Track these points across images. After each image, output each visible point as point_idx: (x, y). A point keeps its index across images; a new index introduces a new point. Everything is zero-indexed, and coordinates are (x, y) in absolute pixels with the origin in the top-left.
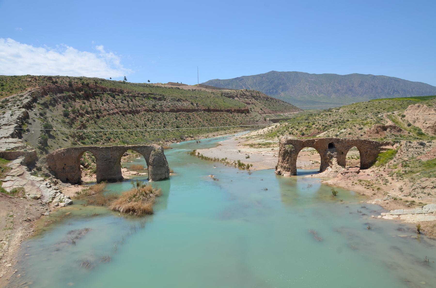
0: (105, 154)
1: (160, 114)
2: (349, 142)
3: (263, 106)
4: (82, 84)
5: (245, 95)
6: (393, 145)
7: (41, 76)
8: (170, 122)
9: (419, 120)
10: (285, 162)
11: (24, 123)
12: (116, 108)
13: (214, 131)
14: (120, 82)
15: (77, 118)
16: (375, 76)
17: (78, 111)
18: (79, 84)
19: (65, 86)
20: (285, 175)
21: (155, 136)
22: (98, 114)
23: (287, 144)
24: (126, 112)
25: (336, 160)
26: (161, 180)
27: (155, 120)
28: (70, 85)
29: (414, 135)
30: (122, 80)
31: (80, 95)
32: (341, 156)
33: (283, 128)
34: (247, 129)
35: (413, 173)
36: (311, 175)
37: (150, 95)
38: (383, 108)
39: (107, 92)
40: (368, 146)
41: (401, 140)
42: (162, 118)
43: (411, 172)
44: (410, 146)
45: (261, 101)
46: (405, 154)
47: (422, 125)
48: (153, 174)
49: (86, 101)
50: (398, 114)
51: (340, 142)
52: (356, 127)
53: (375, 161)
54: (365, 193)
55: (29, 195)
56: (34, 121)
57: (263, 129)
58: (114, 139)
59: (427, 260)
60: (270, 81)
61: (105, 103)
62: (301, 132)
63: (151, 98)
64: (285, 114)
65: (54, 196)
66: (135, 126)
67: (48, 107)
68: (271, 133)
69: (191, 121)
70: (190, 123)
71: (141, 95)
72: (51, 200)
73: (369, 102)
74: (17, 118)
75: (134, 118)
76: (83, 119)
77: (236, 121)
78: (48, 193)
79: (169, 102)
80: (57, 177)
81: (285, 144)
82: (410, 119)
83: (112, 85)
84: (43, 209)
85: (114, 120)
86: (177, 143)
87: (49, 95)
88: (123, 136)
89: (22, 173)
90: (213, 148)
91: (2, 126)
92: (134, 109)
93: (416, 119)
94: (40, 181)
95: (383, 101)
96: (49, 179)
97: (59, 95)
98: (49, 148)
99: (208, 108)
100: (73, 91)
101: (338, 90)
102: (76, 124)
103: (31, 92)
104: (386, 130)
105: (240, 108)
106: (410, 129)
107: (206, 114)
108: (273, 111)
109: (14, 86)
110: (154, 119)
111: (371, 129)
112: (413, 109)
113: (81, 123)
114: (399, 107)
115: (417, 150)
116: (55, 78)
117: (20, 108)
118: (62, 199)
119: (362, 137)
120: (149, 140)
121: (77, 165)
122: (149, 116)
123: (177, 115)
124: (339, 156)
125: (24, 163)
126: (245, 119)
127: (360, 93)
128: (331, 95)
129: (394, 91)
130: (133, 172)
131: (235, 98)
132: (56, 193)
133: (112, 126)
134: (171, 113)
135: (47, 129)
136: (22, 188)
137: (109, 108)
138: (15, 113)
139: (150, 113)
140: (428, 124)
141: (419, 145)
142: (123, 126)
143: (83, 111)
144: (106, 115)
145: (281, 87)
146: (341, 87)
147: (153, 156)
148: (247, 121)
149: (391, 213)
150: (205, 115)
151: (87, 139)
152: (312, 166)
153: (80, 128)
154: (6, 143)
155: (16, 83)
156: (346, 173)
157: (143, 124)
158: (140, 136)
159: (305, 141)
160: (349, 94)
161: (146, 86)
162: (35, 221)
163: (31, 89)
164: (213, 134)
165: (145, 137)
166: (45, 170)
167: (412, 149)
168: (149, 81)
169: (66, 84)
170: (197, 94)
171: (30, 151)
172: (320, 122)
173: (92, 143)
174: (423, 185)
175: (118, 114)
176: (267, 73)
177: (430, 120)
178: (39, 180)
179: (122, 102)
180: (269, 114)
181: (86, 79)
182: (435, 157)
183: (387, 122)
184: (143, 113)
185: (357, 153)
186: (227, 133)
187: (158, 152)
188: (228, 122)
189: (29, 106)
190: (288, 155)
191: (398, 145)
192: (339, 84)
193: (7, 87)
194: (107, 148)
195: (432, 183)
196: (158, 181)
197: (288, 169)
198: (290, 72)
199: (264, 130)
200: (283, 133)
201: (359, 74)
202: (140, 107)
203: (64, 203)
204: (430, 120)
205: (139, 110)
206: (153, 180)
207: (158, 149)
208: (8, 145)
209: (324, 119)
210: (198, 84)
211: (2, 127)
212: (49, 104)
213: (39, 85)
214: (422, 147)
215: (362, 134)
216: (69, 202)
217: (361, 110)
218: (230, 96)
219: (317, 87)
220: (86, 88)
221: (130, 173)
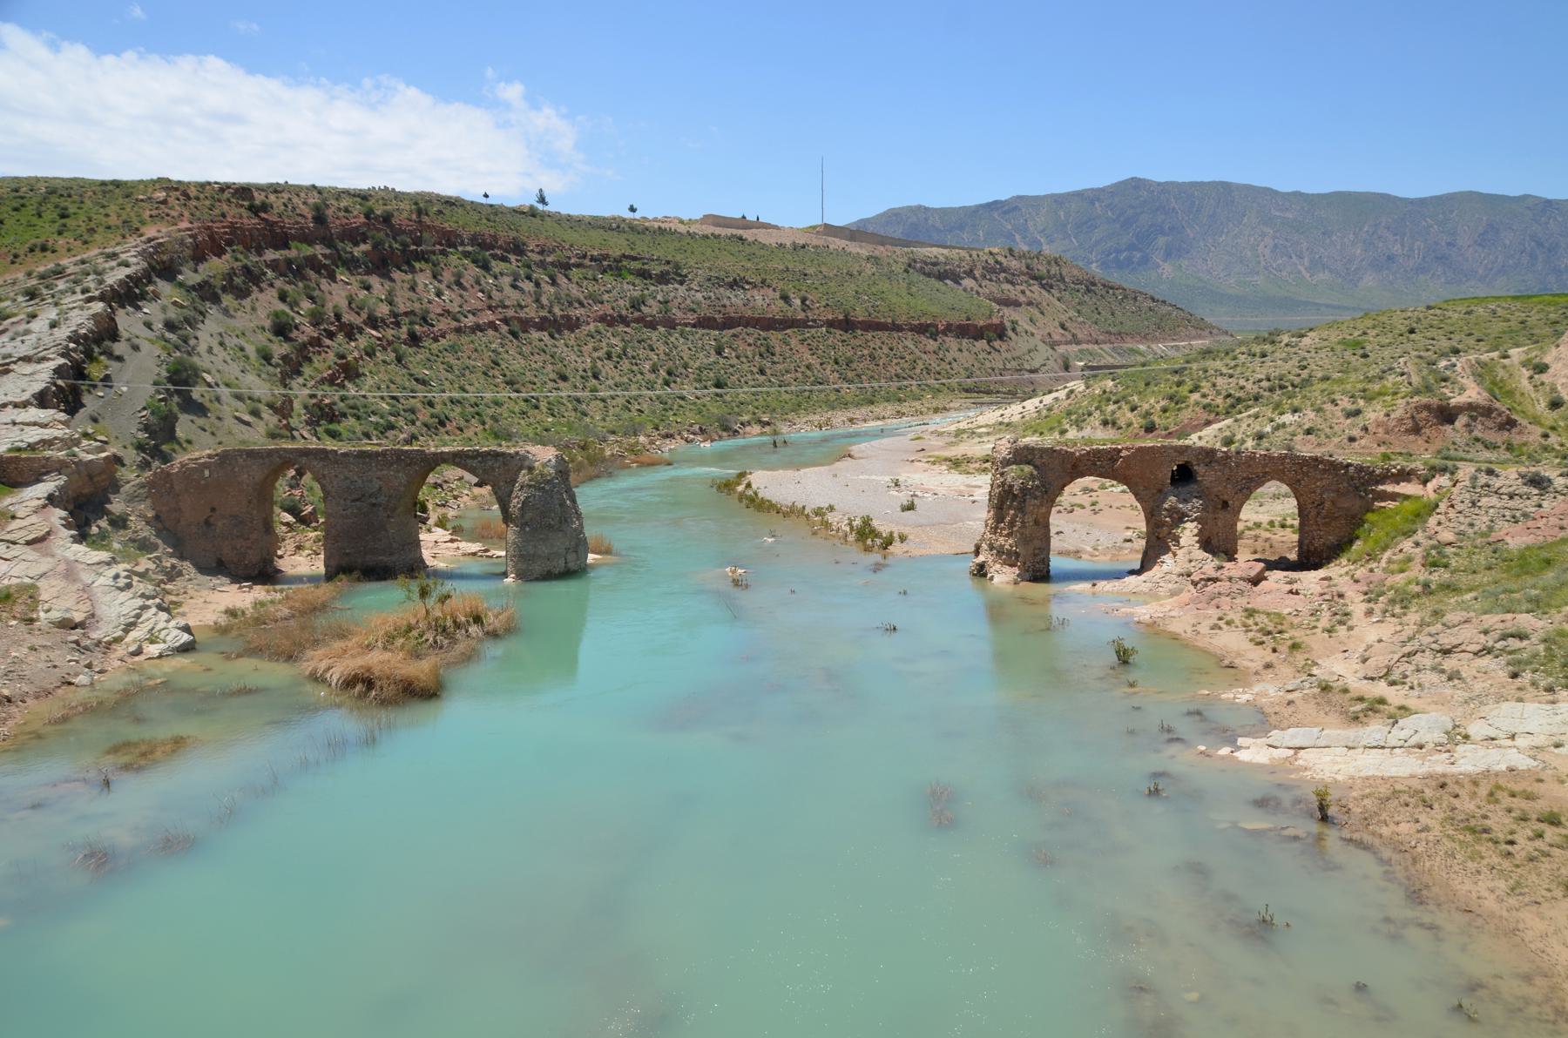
0: (356, 478)
1: (657, 333)
2: (1252, 463)
3: (1072, 313)
4: (367, 216)
5: (1004, 271)
6: (1425, 482)
7: (209, 183)
8: (692, 363)
10: (1001, 529)
11: (95, 354)
12: (490, 308)
13: (858, 405)
14: (516, 211)
15: (328, 342)
16: (1549, 202)
17: (338, 316)
18: (355, 217)
19: (297, 223)
21: (626, 415)
22: (417, 327)
23: (1013, 463)
24: (526, 324)
25: (1196, 531)
26: (548, 576)
27: (634, 358)
28: (320, 219)
29: (1562, 445)
30: (531, 200)
31: (353, 256)
32: (1221, 514)
33: (1093, 398)
34: (986, 399)
35: (1454, 590)
36: (1092, 582)
37: (624, 263)
38: (1477, 335)
39: (460, 249)
41: (1459, 464)
42: (662, 348)
43: (1448, 587)
44: (1489, 486)
45: (1066, 295)
46: (1462, 519)
48: (521, 556)
49: (374, 280)
50: (1524, 357)
51: (1216, 461)
52: (1337, 405)
53: (1351, 542)
54: (1237, 662)
55: (48, 611)
56: (136, 348)
57: (1025, 404)
58: (462, 423)
59: (1268, 918)
60: (1122, 219)
61: (449, 287)
62: (1144, 417)
63: (630, 272)
64: (1154, 346)
65: (132, 620)
66: (553, 376)
67: (216, 299)
68: (1046, 417)
69: (774, 363)
70: (768, 372)
71: (591, 260)
72: (120, 633)
73: (1429, 308)
74: (69, 337)
75: (556, 346)
76: (353, 344)
78: (115, 607)
80: (182, 553)
83: (485, 221)
84: (77, 662)
85: (476, 350)
86: (702, 445)
87: (227, 256)
88: (499, 410)
89: (43, 533)
90: (816, 469)
91: (15, 363)
92: (557, 311)
94: (98, 564)
95: (1486, 308)
96: (149, 559)
97: (270, 255)
98: (176, 447)
99: (845, 316)
100: (328, 241)
101: (1390, 258)
102: (316, 364)
103: (152, 243)
104: (1451, 422)
105: (968, 319)
106: (1555, 421)
107: (834, 338)
108: (1110, 333)
109: (105, 219)
110: (630, 352)
111: (1392, 416)
113: (339, 362)
114: (1544, 332)
115: (1511, 504)
116: (263, 190)
117: (90, 300)
118: (160, 631)
119: (1353, 444)
120: (599, 428)
121: (255, 512)
122: (614, 341)
123: (723, 340)
124: (1211, 516)
125: (60, 496)
126: (987, 362)
127: (1480, 271)
130: (469, 544)
131: (962, 282)
132: (144, 608)
133: (464, 375)
134: (701, 331)
135: (181, 378)
136: (33, 586)
137: (461, 306)
138: (66, 319)
139: (621, 328)
141: (1525, 484)
142: (508, 373)
143: (359, 314)
144: (445, 333)
146: (1402, 245)
148: (993, 370)
149: (1270, 741)
150: (830, 342)
151: (352, 421)
152: (1121, 548)
153: (331, 381)
154: (14, 423)
155: (112, 209)
156: (1209, 580)
157: (585, 371)
158: (565, 414)
159: (1084, 455)
161: (618, 227)
162: (30, 701)
163: (159, 231)
164: (852, 416)
165: (588, 420)
166: (141, 525)
167: (1494, 500)
168: (632, 209)
169: (305, 214)
170: (809, 263)
171: (91, 457)
172: (1220, 381)
173: (367, 436)
174: (1447, 640)
175: (496, 329)
178: (96, 560)
179: (514, 287)
180: (1090, 346)
181: (383, 199)
182: (1562, 534)
183: (1463, 389)
185: (1290, 506)
186: (904, 414)
187: (542, 475)
188: (918, 371)
189: (129, 295)
190: (1011, 503)
191: (1443, 480)
192: (1396, 235)
193: (77, 223)
194: (362, 455)
195: (1482, 636)
196: (537, 579)
197: (1009, 558)
199: (1024, 408)
200: (1085, 420)
203: (162, 646)
205: (578, 319)
206: (522, 576)
207: (544, 465)
208: (18, 432)
209: (1239, 370)
210: (820, 223)
211: (13, 366)
212: (224, 289)
213: (192, 215)
214: (1536, 491)
215: (1356, 432)
216: (182, 641)
217: (1387, 341)
218: (945, 271)
220: (379, 230)
221: (458, 548)
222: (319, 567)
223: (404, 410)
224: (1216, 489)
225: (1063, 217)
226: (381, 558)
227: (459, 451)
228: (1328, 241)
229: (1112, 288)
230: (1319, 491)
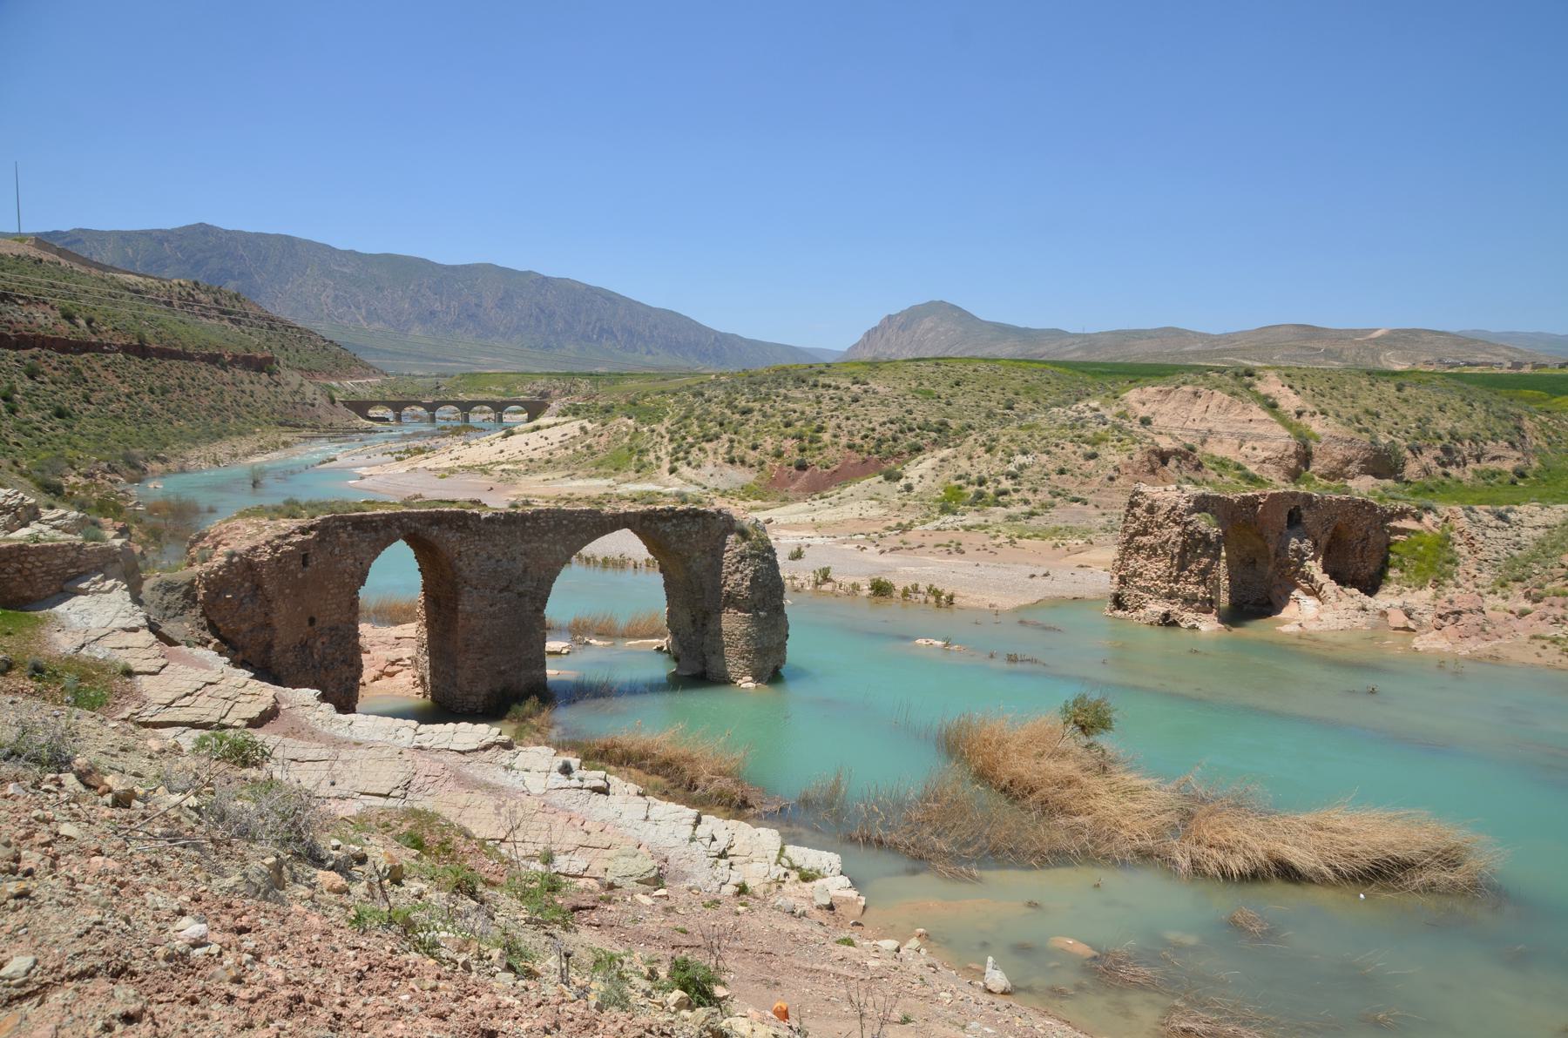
10: (1186, 578)
16: (546, 278)
60: (192, 261)
64: (342, 382)
81: (1190, 512)
94: (486, 748)
99: (140, 342)
104: (1166, 465)
127: (501, 329)
128: (409, 329)
146: (442, 304)
176: (179, 229)
198: (268, 235)
206: (757, 678)
219: (361, 298)
225: (130, 253)
226: (534, 672)
227: (650, 511)
228: (380, 296)
230: (1365, 529)
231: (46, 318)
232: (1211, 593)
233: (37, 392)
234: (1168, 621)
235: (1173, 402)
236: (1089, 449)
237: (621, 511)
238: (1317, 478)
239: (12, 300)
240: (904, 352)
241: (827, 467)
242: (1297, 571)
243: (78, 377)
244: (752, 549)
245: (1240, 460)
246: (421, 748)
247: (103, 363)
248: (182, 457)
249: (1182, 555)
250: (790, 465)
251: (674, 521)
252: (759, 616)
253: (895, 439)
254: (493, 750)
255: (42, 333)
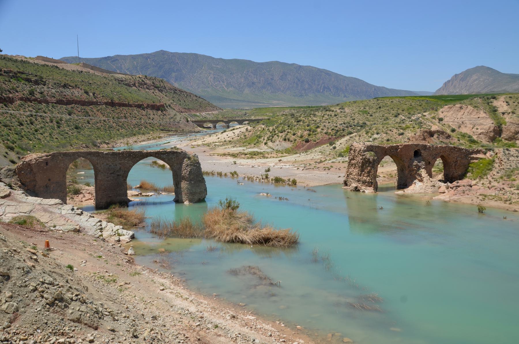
3: (171, 101)
9: (465, 125)
16: (300, 66)
20: (367, 191)
23: (367, 151)
25: (426, 172)
37: (19, 75)
40: (457, 155)
44: (509, 154)
47: (471, 130)
48: (191, 193)
51: (427, 149)
60: (158, 66)
64: (201, 113)
71: (5, 73)
77: (152, 121)
79: (52, 89)
81: (364, 151)
82: (452, 123)
93: (461, 123)
94: (56, 204)
99: (111, 101)
101: (253, 83)
104: (433, 136)
111: (417, 135)
112: (454, 111)
127: (282, 89)
129: (325, 87)
134: (60, 106)
140: (479, 130)
145: (174, 74)
146: (257, 79)
147: (187, 166)
159: (388, 148)
160: (267, 89)
177: (481, 124)
184: (19, 102)
186: (150, 139)
187: (195, 160)
190: (369, 164)
196: (196, 202)
201: (280, 62)
202: (11, 93)
204: (481, 124)
206: (190, 201)
219: (224, 78)
222: (92, 203)
223: (67, 138)
224: (427, 158)
225: (135, 64)
226: (122, 197)
228: (232, 77)
229: (182, 92)
231: (78, 93)
232: (371, 180)
233: (70, 120)
234: (357, 189)
235: (452, 111)
236: (402, 131)
237: (149, 152)
238: (503, 140)
239: (67, 87)
240: (463, 91)
241: (315, 141)
242: (416, 173)
243: (87, 114)
244: (191, 163)
245: (471, 134)
246: (41, 204)
247: (97, 109)
248: (115, 142)
249: (362, 167)
250: (303, 141)
251: (167, 155)
252: (191, 183)
253: (343, 130)
254: (58, 205)
255: (76, 99)
